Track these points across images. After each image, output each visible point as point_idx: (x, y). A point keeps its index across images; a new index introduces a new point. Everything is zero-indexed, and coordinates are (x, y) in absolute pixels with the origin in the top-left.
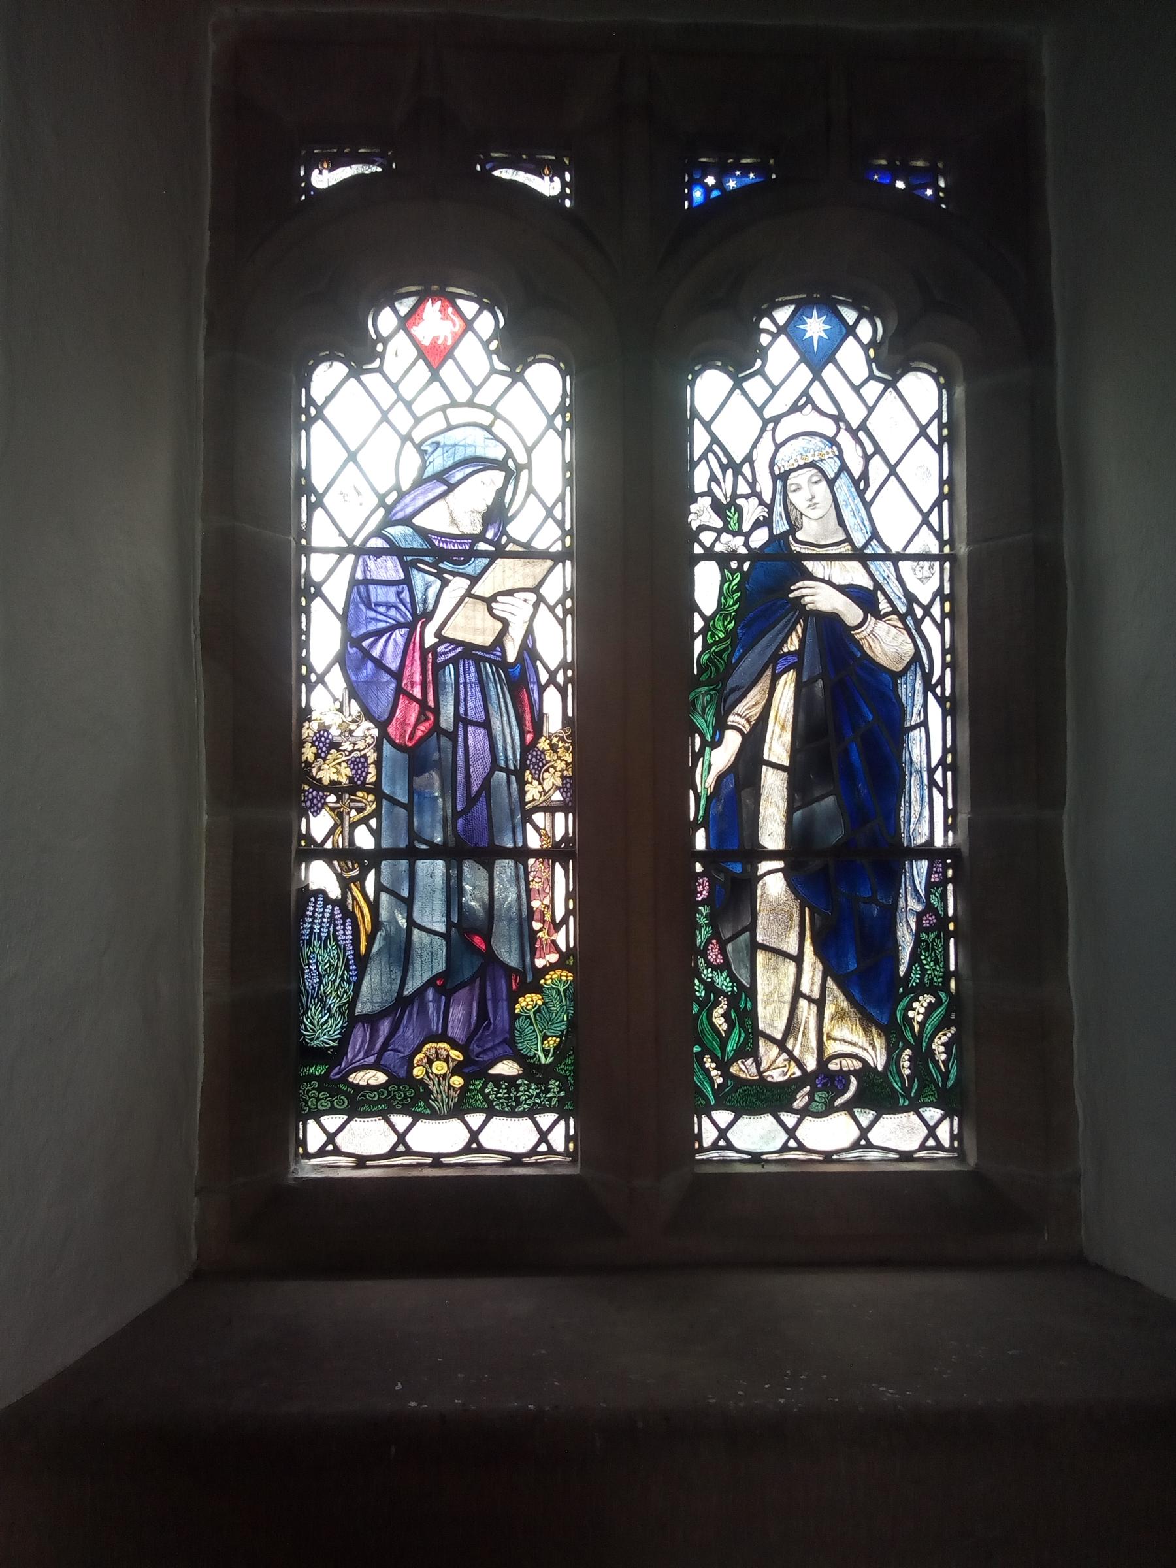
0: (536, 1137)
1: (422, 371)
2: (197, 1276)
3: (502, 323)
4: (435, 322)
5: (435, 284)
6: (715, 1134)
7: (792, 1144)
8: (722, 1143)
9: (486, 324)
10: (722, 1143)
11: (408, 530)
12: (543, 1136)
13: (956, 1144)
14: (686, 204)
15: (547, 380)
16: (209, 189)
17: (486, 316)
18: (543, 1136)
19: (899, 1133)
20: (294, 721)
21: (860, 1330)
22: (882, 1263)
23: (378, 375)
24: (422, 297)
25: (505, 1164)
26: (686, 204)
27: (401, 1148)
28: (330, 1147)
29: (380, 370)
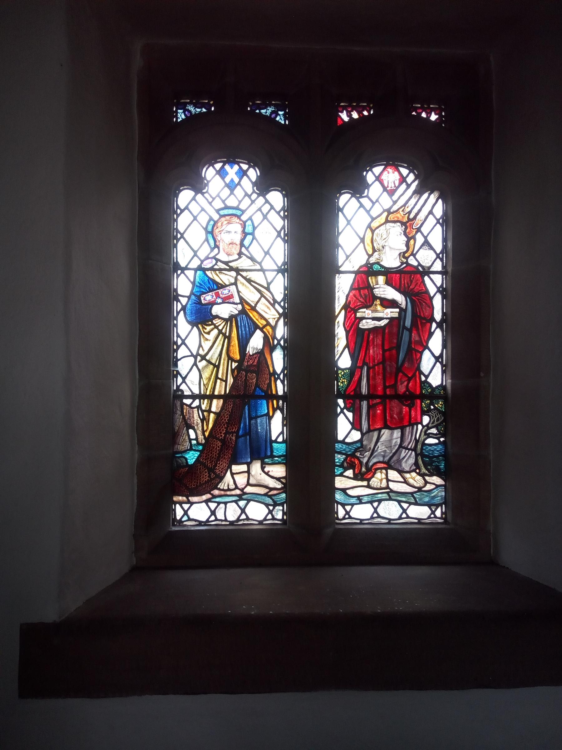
0: (239, 511)
1: (227, 191)
2: (135, 569)
3: (259, 174)
4: (391, 177)
5: (393, 162)
6: (182, 513)
7: (375, 515)
8: (432, 516)
9: (253, 174)
10: (432, 516)
11: (209, 260)
12: (213, 513)
13: (444, 516)
14: (175, 119)
15: (277, 198)
16: (135, 106)
17: (251, 170)
18: (213, 513)
19: (419, 512)
20: (271, 340)
21: (408, 588)
22: (259, 565)
23: (366, 199)
24: (386, 166)
25: (197, 525)
26: (175, 119)
27: (375, 515)
28: (243, 517)
29: (367, 196)
